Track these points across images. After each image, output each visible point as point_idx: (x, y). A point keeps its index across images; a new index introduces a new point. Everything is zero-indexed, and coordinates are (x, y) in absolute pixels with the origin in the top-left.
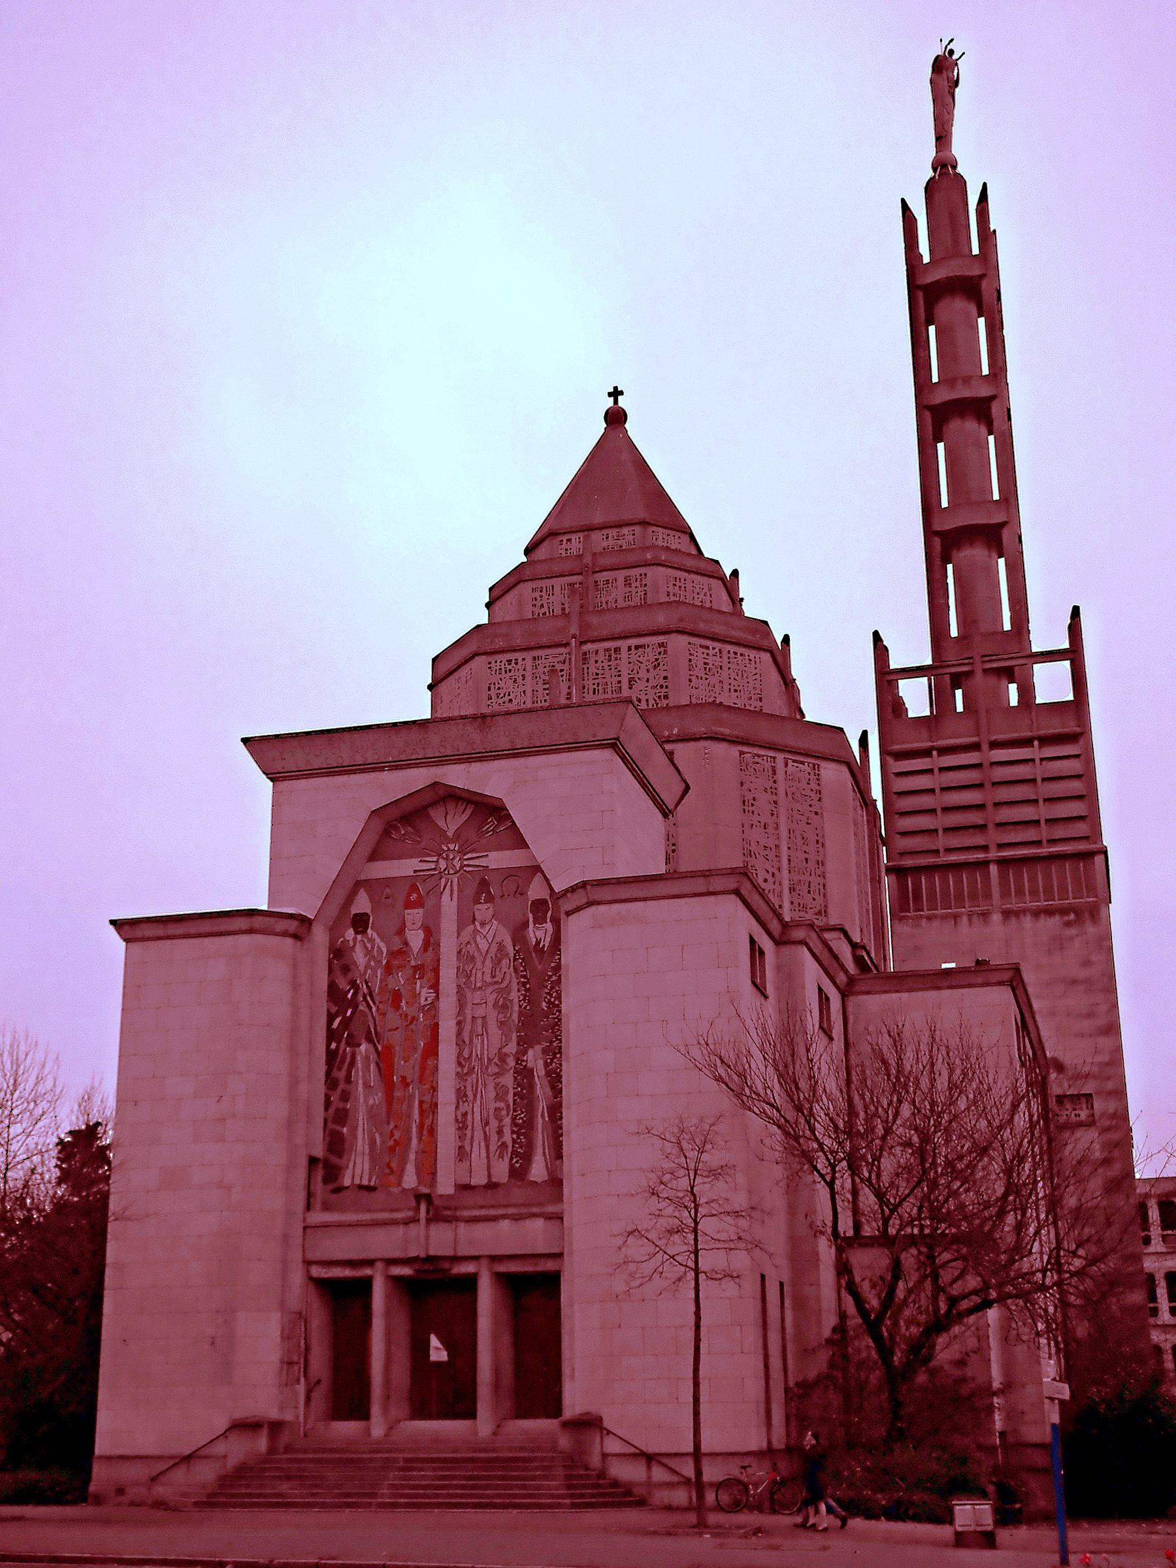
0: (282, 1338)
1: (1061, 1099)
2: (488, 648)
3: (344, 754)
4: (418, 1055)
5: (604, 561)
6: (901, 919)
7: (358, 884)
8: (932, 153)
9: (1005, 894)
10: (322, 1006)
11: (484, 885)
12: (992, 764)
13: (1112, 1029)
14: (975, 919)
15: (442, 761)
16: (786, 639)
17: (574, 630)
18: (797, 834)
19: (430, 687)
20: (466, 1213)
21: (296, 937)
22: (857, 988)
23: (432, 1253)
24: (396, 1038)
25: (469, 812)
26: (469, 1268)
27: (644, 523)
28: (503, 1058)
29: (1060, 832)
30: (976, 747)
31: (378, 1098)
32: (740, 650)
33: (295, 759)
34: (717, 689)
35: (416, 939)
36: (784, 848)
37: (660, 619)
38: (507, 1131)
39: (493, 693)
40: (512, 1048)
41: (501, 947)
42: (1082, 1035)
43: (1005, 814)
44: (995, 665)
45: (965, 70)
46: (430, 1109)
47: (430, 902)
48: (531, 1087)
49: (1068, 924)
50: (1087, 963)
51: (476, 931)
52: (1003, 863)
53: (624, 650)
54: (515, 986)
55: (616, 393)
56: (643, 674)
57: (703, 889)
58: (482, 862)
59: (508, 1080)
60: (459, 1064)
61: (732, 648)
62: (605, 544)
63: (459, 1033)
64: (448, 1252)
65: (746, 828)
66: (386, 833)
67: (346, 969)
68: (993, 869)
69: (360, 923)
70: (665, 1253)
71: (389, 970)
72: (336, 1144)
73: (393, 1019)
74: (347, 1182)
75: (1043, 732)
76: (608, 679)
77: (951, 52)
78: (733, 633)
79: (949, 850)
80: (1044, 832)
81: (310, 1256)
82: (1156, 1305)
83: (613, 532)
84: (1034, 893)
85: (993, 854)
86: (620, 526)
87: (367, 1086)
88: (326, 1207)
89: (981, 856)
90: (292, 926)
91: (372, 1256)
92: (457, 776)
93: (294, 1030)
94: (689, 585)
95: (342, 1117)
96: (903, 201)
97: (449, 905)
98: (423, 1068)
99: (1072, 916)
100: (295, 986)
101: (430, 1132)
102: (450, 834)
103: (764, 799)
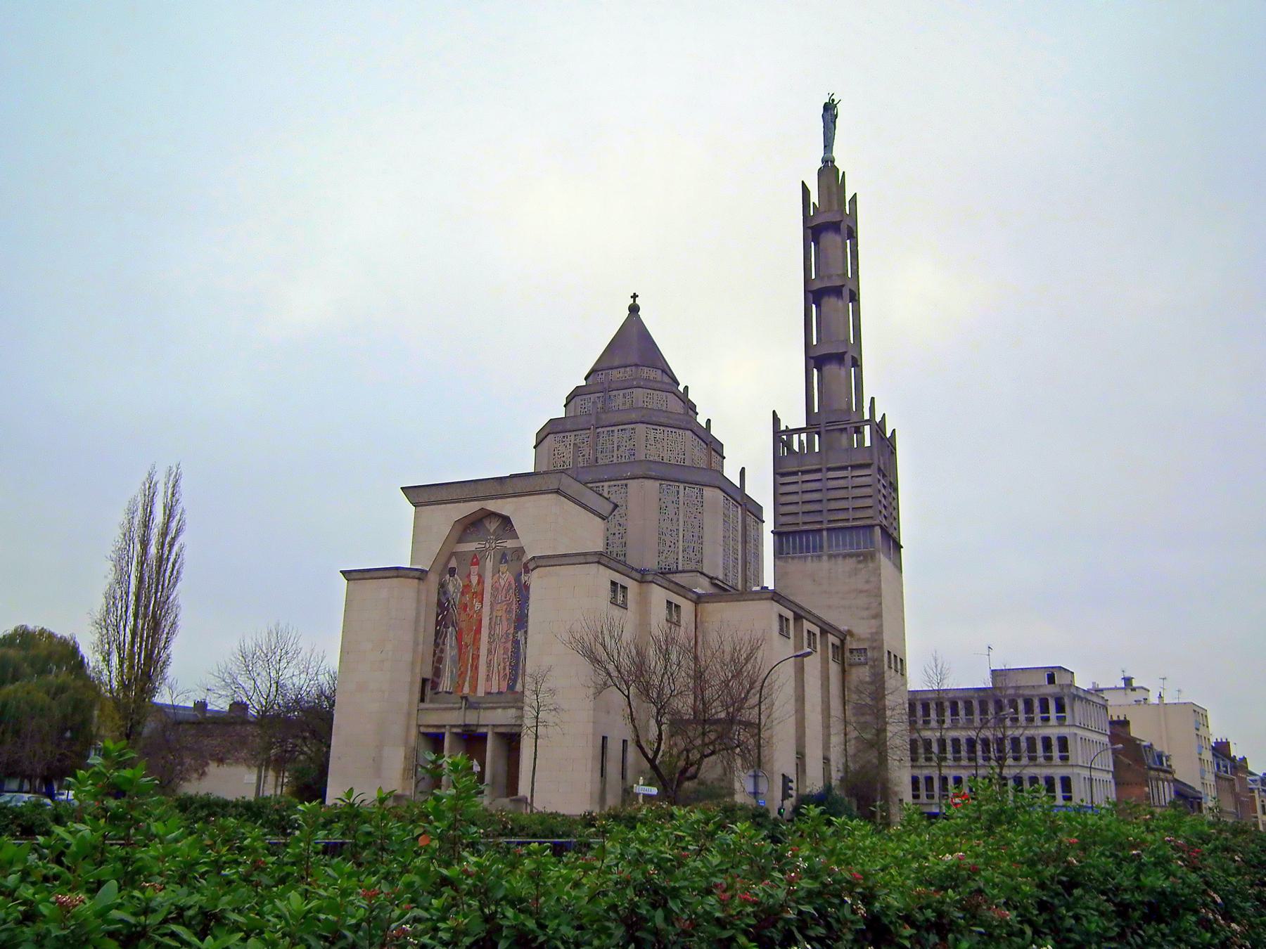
0: (405, 757)
1: (851, 651)
2: (554, 431)
3: (444, 495)
4: (473, 633)
5: (613, 386)
6: (779, 558)
7: (453, 554)
8: (821, 154)
9: (830, 546)
10: (434, 609)
11: (504, 556)
12: (828, 479)
13: (878, 616)
14: (814, 559)
15: (486, 498)
16: (709, 421)
17: (593, 422)
18: (689, 523)
19: (535, 447)
20: (484, 706)
21: (419, 579)
22: (702, 600)
23: (467, 723)
24: (463, 625)
25: (500, 521)
26: (483, 730)
27: (636, 365)
28: (507, 635)
29: (859, 514)
30: (819, 470)
31: (455, 652)
32: (674, 430)
33: (424, 497)
34: (661, 450)
35: (474, 580)
36: (681, 530)
37: (634, 416)
38: (507, 668)
39: (556, 452)
40: (512, 631)
41: (510, 584)
42: (863, 619)
43: (834, 505)
44: (839, 427)
45: (840, 109)
46: (476, 657)
47: (481, 563)
48: (519, 647)
49: (859, 562)
50: (867, 582)
51: (499, 576)
52: (828, 529)
53: (616, 431)
54: (514, 603)
55: (635, 296)
56: (624, 444)
57: (584, 561)
58: (504, 545)
59: (509, 645)
60: (489, 637)
61: (670, 429)
62: (618, 376)
63: (490, 623)
64: (475, 723)
65: (662, 521)
66: (465, 530)
67: (445, 593)
68: (825, 533)
69: (452, 572)
70: (537, 727)
71: (463, 594)
72: (437, 672)
73: (463, 617)
74: (440, 690)
75: (853, 463)
76: (608, 446)
77: (833, 100)
78: (671, 422)
79: (805, 523)
80: (851, 514)
81: (420, 723)
82: (1067, 754)
83: (622, 370)
84: (844, 545)
85: (825, 526)
86: (626, 367)
87: (451, 646)
88: (432, 701)
89: (818, 526)
90: (417, 574)
91: (445, 723)
92: (492, 506)
93: (417, 621)
94: (655, 397)
95: (440, 660)
96: (803, 182)
97: (489, 564)
98: (474, 639)
99: (862, 558)
100: (418, 601)
101: (475, 668)
102: (491, 531)
103: (671, 509)
